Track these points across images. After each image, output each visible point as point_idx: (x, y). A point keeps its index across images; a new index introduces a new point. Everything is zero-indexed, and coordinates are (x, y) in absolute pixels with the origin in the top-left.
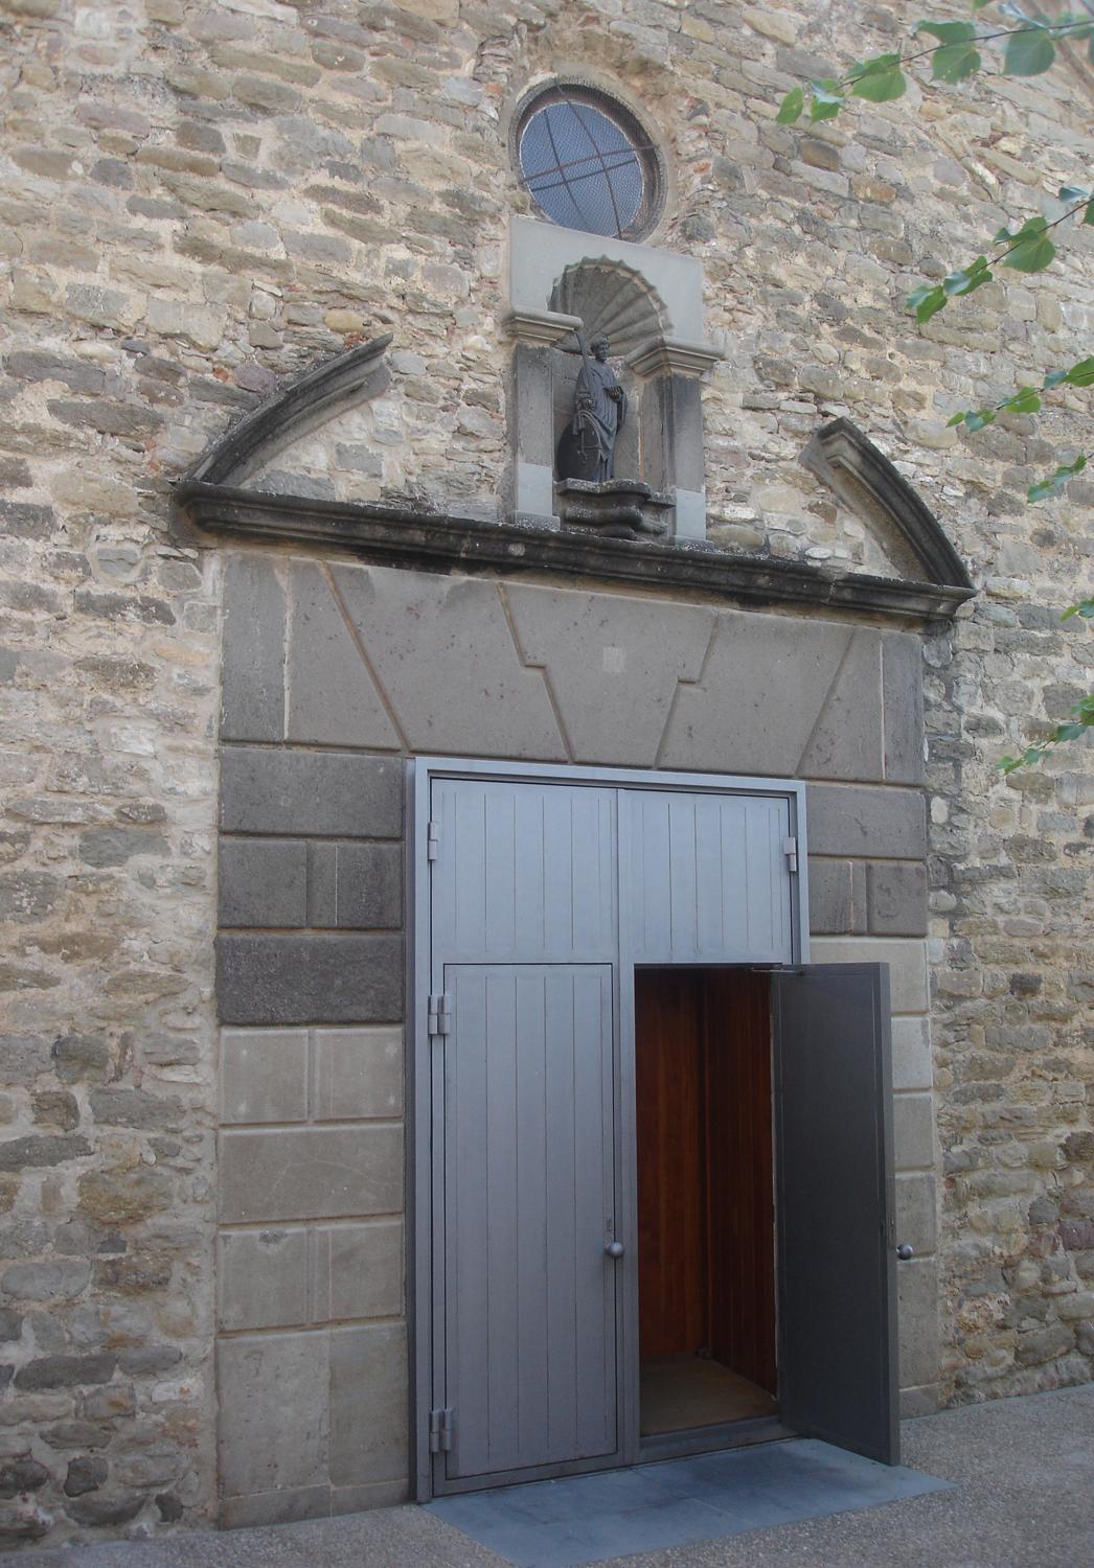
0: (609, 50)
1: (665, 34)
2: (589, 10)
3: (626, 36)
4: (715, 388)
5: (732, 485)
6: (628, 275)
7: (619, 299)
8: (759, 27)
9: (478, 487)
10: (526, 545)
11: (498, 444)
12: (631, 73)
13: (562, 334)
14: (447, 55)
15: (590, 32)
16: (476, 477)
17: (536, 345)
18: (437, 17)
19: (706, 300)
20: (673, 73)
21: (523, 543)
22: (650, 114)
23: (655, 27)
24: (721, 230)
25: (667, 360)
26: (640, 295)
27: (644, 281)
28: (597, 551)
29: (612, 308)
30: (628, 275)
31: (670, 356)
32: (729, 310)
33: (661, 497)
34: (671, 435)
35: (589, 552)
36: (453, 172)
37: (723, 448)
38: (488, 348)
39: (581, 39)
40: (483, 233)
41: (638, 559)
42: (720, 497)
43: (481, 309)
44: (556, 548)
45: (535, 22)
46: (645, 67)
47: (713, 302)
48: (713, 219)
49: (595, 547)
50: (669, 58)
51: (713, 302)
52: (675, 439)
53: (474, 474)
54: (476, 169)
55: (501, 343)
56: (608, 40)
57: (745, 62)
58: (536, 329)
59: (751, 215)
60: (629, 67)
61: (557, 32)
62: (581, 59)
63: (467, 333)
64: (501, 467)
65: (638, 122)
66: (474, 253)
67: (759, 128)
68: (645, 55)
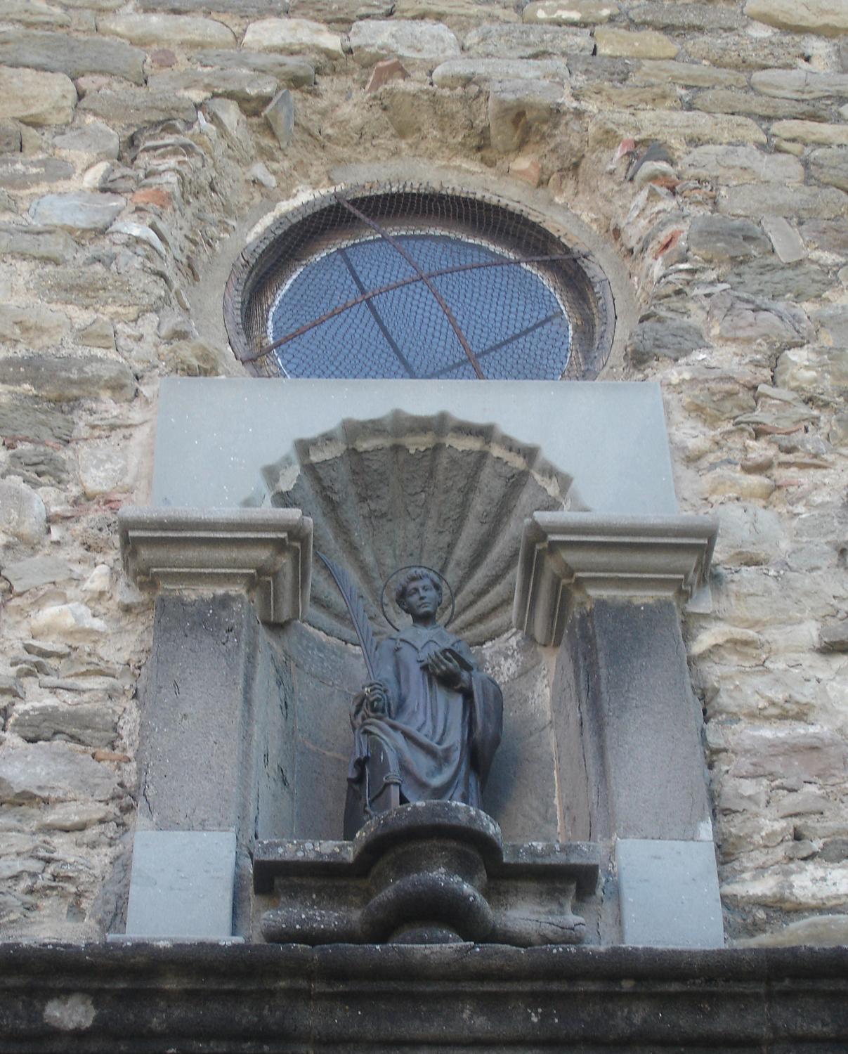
0: (444, 119)
1: (560, 63)
2: (378, 58)
3: (468, 81)
4: (734, 621)
5: (812, 821)
6: (474, 444)
7: (479, 505)
8: (783, 18)
9: (31, 908)
10: (97, 997)
11: (97, 810)
12: (507, 152)
13: (263, 554)
14: (42, 163)
15: (391, 93)
16: (25, 883)
17: (207, 591)
18: (23, 113)
19: (692, 459)
20: (579, 114)
21: (84, 991)
22: (565, 208)
23: (535, 56)
24: (716, 331)
25: (570, 572)
26: (517, 481)
27: (510, 445)
28: (318, 987)
29: (472, 530)
30: (474, 444)
31: (570, 557)
32: (761, 468)
33: (550, 850)
34: (599, 731)
35: (294, 995)
36: (26, 329)
37: (772, 744)
38: (98, 624)
39: (378, 112)
40: (90, 419)
41: (458, 996)
42: (780, 852)
43: (79, 552)
44: (190, 995)
45: (252, 92)
46: (526, 124)
47: (711, 458)
48: (697, 318)
49: (309, 976)
50: (567, 91)
51: (711, 458)
52: (608, 731)
53: (16, 877)
54: (82, 317)
55: (127, 609)
56: (435, 100)
57: (758, 76)
58: (192, 554)
59: (799, 297)
60: (496, 138)
61: (323, 113)
62: (396, 153)
63: (38, 603)
64: (101, 859)
65: (534, 225)
66: (65, 454)
67: (806, 164)
68: (510, 97)
